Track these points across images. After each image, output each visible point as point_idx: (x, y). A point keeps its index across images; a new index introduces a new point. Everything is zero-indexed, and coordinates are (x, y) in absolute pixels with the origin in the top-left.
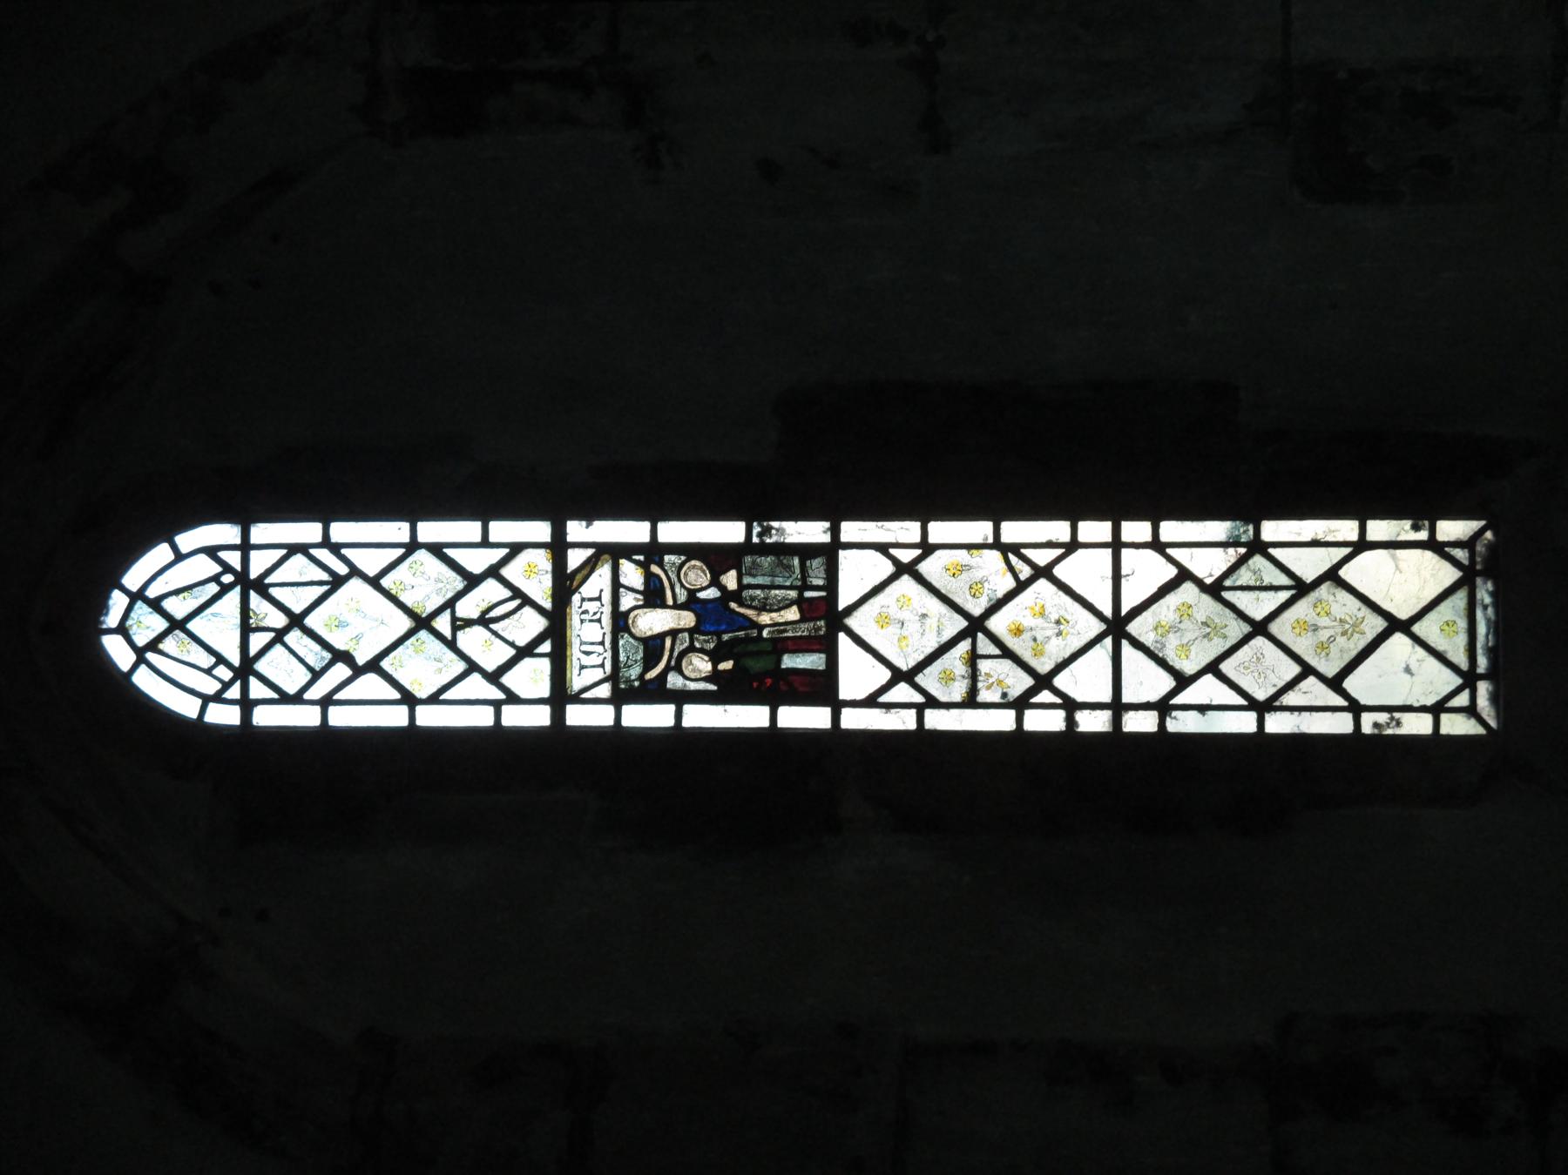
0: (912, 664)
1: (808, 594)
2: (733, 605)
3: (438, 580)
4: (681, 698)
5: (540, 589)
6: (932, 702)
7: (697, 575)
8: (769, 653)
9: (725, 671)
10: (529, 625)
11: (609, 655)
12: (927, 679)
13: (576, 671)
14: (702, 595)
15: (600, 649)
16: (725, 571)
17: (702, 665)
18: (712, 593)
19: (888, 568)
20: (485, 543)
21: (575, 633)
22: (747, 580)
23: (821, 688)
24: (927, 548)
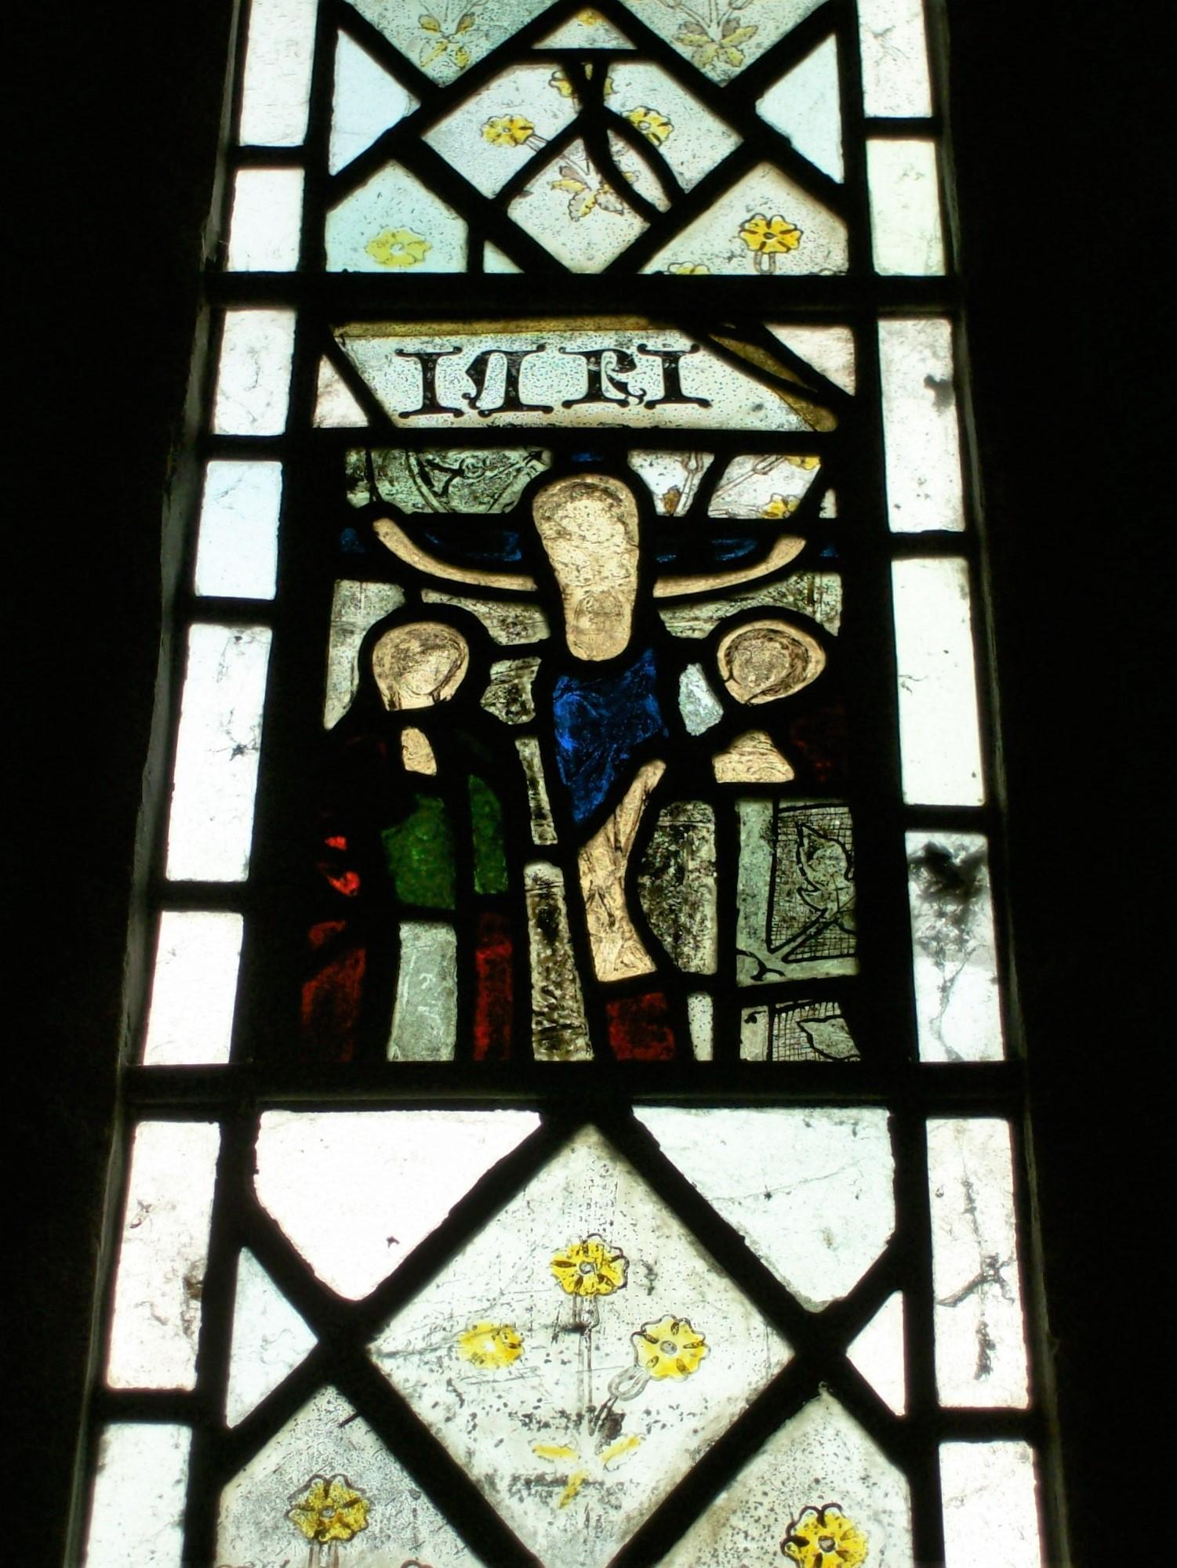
0: (400, 1373)
1: (701, 1013)
2: (652, 775)
3: (729, 27)
4: (294, 626)
5: (705, 248)
6: (220, 1454)
7: (768, 665)
8: (462, 884)
9: (396, 749)
10: (579, 225)
11: (471, 419)
12: (326, 1438)
13: (412, 345)
14: (692, 681)
15: (493, 395)
16: (784, 747)
17: (423, 674)
18: (698, 704)
19: (821, 1279)
20: (859, 128)
21: (553, 340)
22: (753, 816)
23: (314, 1041)
24: (915, 1437)
